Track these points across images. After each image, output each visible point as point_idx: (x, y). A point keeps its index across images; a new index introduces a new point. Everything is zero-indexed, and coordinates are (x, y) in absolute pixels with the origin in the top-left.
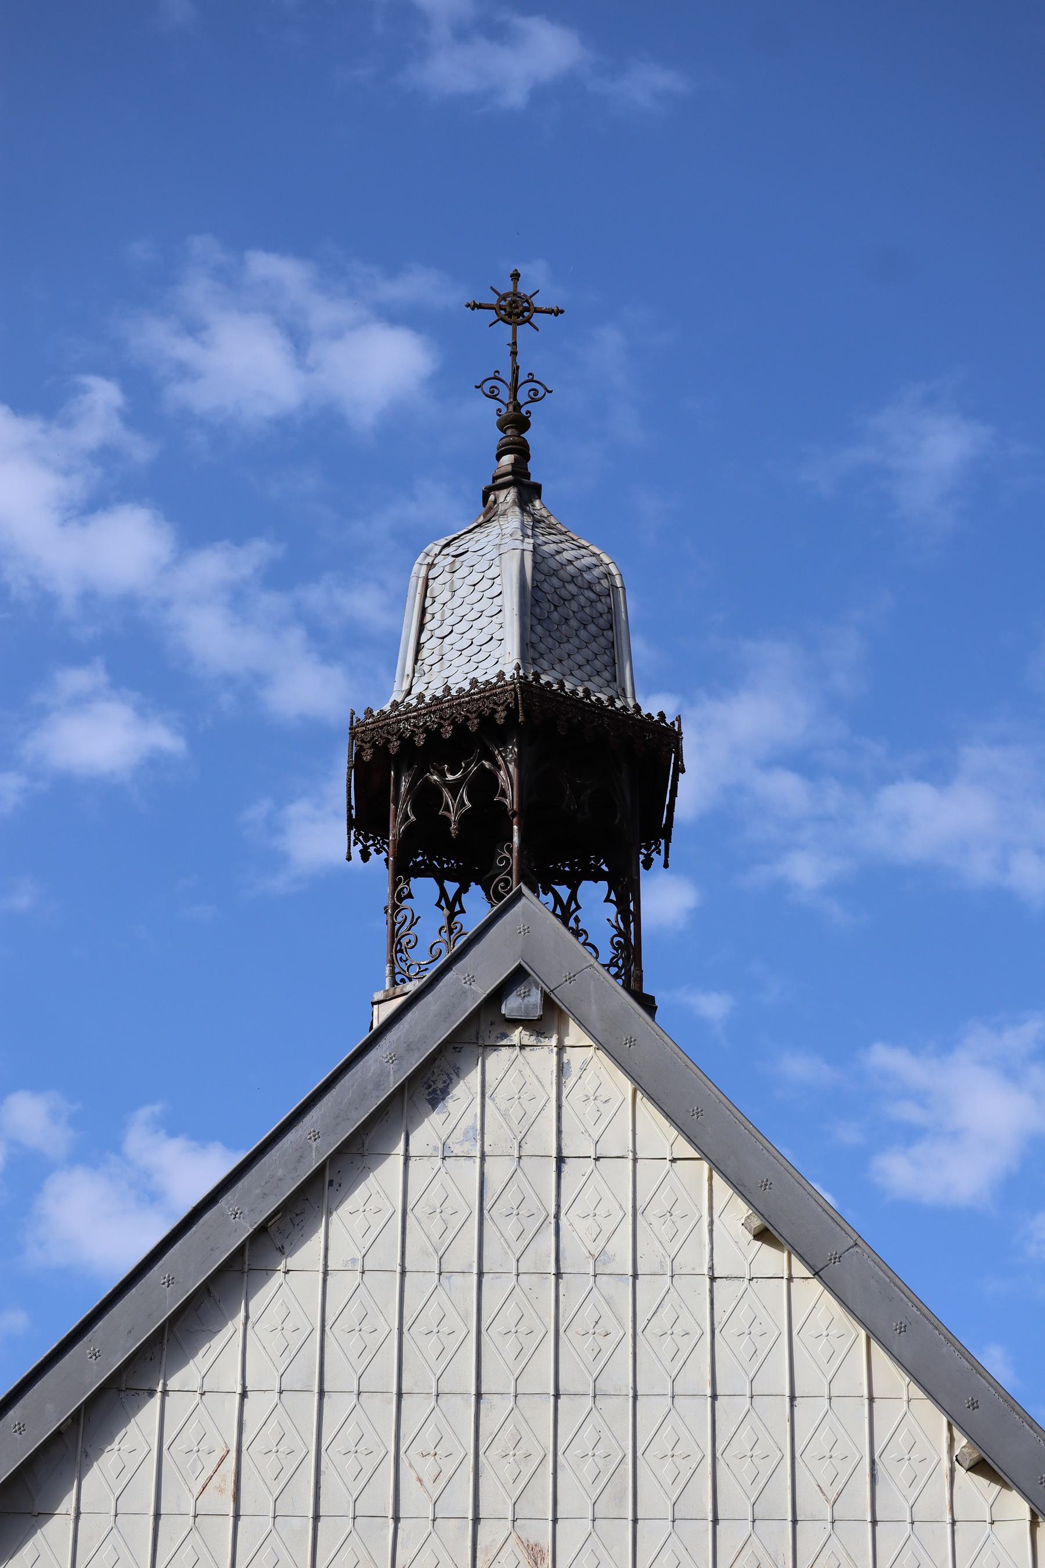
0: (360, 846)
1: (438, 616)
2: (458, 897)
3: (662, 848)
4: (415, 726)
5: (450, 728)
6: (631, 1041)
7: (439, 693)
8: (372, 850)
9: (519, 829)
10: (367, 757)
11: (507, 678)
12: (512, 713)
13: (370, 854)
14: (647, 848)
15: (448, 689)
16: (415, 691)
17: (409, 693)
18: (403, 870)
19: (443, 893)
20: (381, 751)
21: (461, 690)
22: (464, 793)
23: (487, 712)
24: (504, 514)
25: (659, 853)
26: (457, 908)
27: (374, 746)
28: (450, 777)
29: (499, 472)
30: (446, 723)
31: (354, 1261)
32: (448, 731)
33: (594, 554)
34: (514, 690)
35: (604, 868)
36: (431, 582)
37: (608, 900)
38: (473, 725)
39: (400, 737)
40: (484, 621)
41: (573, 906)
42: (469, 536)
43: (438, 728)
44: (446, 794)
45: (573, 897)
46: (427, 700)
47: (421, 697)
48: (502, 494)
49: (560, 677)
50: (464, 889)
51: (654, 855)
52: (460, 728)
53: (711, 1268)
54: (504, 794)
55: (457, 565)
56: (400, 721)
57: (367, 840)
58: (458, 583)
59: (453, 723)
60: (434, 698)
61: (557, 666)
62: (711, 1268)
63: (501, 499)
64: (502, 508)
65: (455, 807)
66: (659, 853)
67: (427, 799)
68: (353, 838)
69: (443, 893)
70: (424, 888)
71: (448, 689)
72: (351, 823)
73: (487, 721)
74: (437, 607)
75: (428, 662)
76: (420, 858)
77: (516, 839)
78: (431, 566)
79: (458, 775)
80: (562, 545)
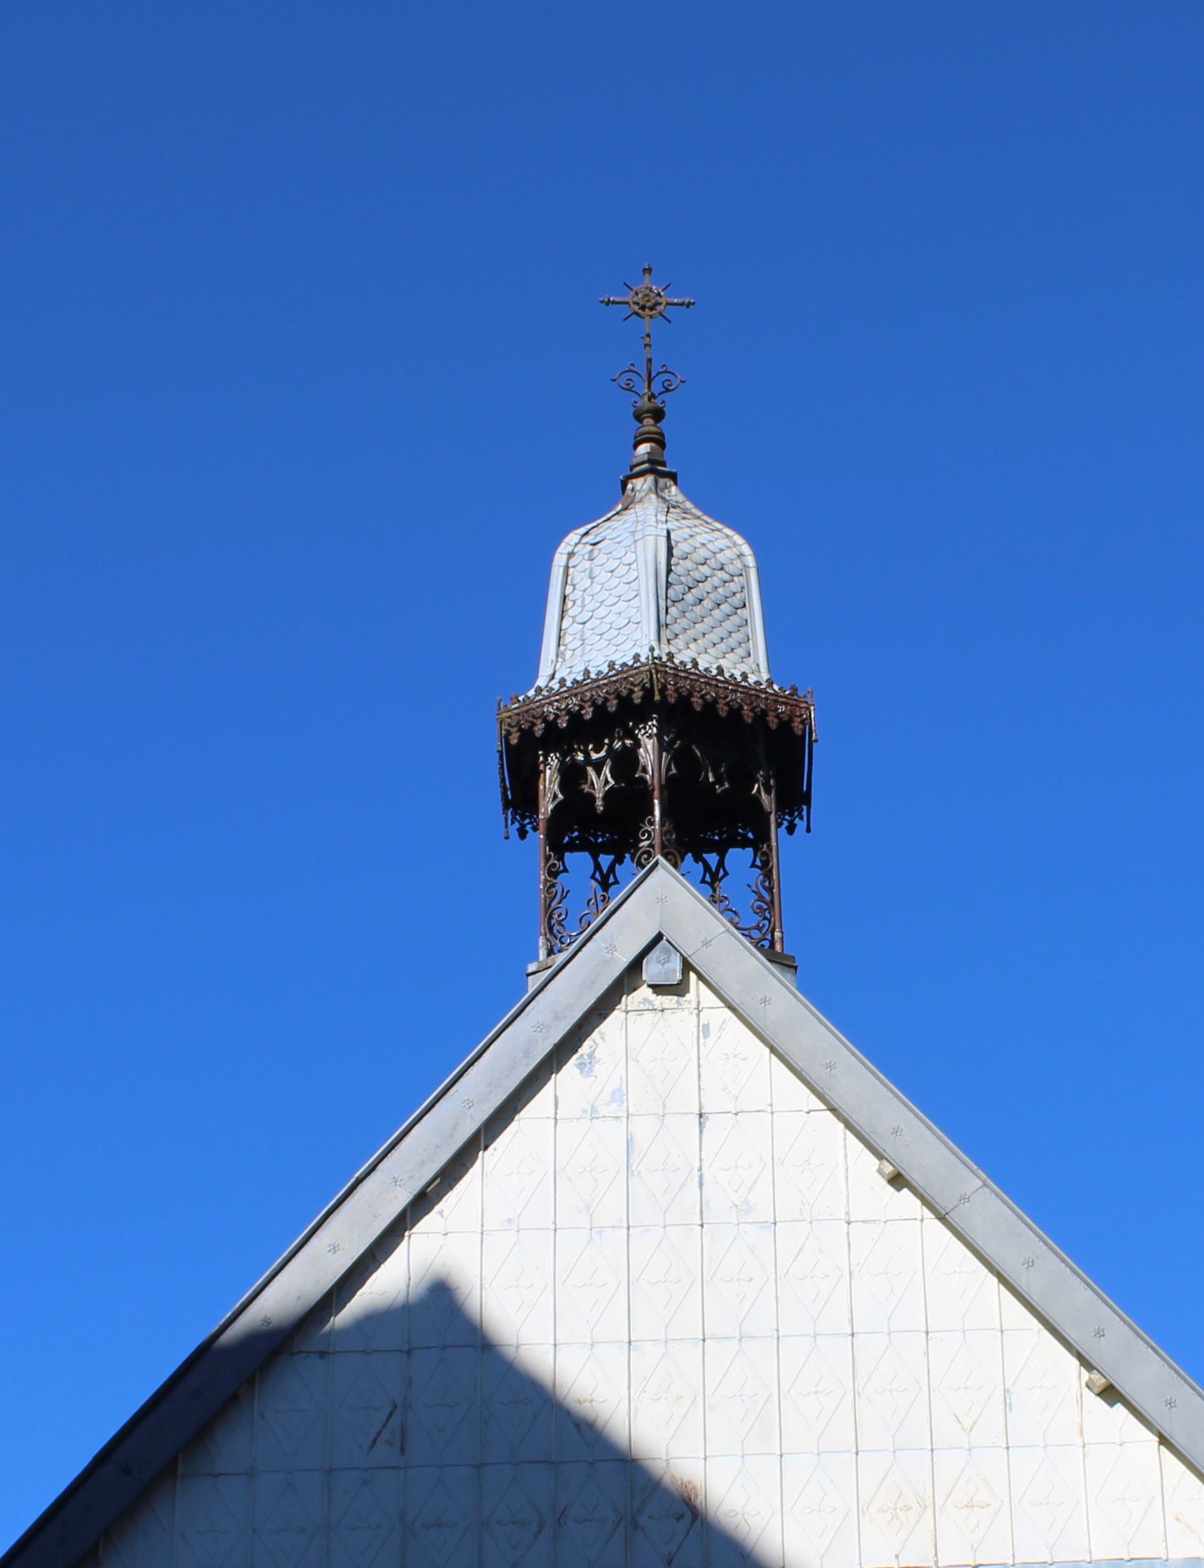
0: (517, 825)
1: (579, 603)
2: (612, 869)
3: (804, 813)
4: (558, 709)
5: (615, 702)
6: (765, 1001)
7: (580, 678)
8: (528, 828)
9: (661, 804)
10: (514, 740)
11: (643, 659)
12: (648, 693)
13: (527, 832)
14: (791, 814)
15: (587, 672)
16: (558, 677)
17: (553, 677)
18: (557, 846)
19: (598, 867)
20: (526, 734)
21: (600, 673)
22: (606, 770)
23: (625, 693)
24: (640, 501)
25: (801, 818)
26: (612, 880)
27: (520, 730)
28: (594, 756)
29: (635, 461)
30: (539, 721)
31: (509, 1221)
32: (588, 713)
33: (727, 536)
34: (650, 671)
35: (750, 835)
36: (571, 570)
37: (753, 865)
38: (612, 706)
39: (545, 720)
40: (622, 605)
41: (721, 873)
42: (608, 524)
43: (579, 711)
44: (591, 772)
45: (721, 864)
46: (569, 684)
47: (562, 682)
48: (638, 483)
49: (695, 656)
50: (619, 860)
51: (797, 821)
52: (600, 709)
53: (848, 1213)
54: (645, 770)
55: (596, 553)
56: (543, 706)
57: (523, 818)
58: (596, 571)
59: (594, 704)
60: (575, 681)
61: (692, 646)
62: (848, 1213)
63: (638, 487)
64: (638, 496)
65: (600, 783)
66: (801, 818)
67: (572, 777)
68: (510, 817)
69: (598, 867)
70: (579, 862)
71: (587, 672)
72: (507, 804)
73: (625, 701)
74: (577, 594)
75: (571, 646)
76: (576, 834)
77: (657, 813)
78: (571, 555)
79: (603, 753)
80: (697, 530)
